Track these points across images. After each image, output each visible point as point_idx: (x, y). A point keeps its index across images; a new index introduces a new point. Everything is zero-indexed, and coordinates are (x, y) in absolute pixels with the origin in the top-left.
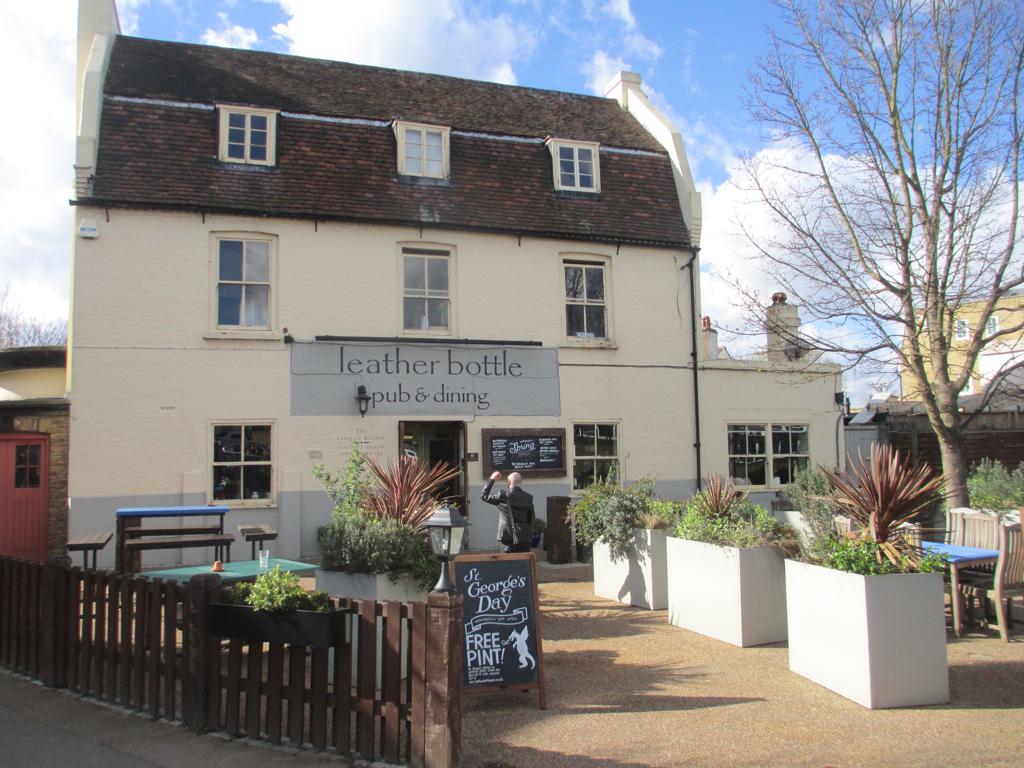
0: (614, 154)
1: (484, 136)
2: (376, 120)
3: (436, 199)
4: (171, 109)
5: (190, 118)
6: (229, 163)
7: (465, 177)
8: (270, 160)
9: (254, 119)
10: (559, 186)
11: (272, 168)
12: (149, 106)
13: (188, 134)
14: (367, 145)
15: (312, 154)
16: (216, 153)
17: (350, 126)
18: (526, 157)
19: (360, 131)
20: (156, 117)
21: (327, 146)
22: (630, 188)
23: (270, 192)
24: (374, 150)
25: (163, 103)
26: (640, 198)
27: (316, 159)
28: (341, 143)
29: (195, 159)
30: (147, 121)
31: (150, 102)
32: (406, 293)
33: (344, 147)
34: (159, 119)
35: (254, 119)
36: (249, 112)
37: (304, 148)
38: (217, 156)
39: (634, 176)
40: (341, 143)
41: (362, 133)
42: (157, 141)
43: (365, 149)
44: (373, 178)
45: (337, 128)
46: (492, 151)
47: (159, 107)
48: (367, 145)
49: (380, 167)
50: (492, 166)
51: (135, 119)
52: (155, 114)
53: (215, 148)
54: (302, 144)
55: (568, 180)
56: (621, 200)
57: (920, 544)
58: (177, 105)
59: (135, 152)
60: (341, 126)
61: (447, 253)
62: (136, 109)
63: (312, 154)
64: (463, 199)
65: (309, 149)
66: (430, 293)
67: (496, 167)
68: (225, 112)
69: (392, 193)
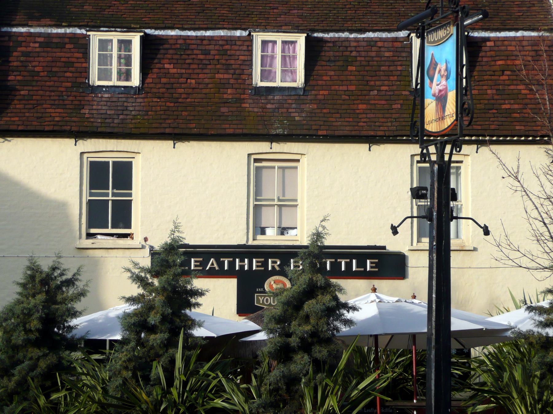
0: (488, 39)
1: (345, 35)
2: (236, 29)
3: (288, 109)
4: (49, 35)
5: (66, 43)
6: (98, 86)
7: (320, 83)
8: (135, 81)
9: (120, 42)
10: (258, 81)
11: (138, 90)
12: (30, 34)
13: (63, 60)
14: (227, 57)
15: (175, 71)
16: (88, 78)
17: (211, 38)
18: (387, 54)
19: (221, 43)
20: (37, 45)
21: (187, 61)
22: (502, 78)
23: (133, 113)
24: (232, 62)
25: (42, 30)
26: (512, 87)
27: (176, 75)
28: (202, 57)
29: (69, 85)
30: (29, 49)
31: (32, 30)
32: (130, 195)
33: (204, 62)
34: (39, 47)
35: (120, 42)
36: (115, 36)
37: (167, 66)
38: (89, 81)
39: (509, 62)
40: (202, 57)
41: (222, 45)
42: (37, 69)
43: (224, 62)
44: (229, 91)
45: (199, 42)
46: (351, 52)
47: (39, 35)
48: (227, 57)
49: (236, 79)
50: (350, 68)
51: (19, 49)
52: (36, 42)
53: (86, 71)
54: (167, 61)
55: (104, 74)
56: (489, 92)
57: (159, 394)
58: (55, 31)
59: (18, 81)
60: (203, 39)
61: (298, 161)
62: (20, 39)
63: (175, 71)
64: (315, 106)
65: (172, 66)
66: (114, 195)
67: (354, 68)
68: (259, 37)
69: (247, 105)
